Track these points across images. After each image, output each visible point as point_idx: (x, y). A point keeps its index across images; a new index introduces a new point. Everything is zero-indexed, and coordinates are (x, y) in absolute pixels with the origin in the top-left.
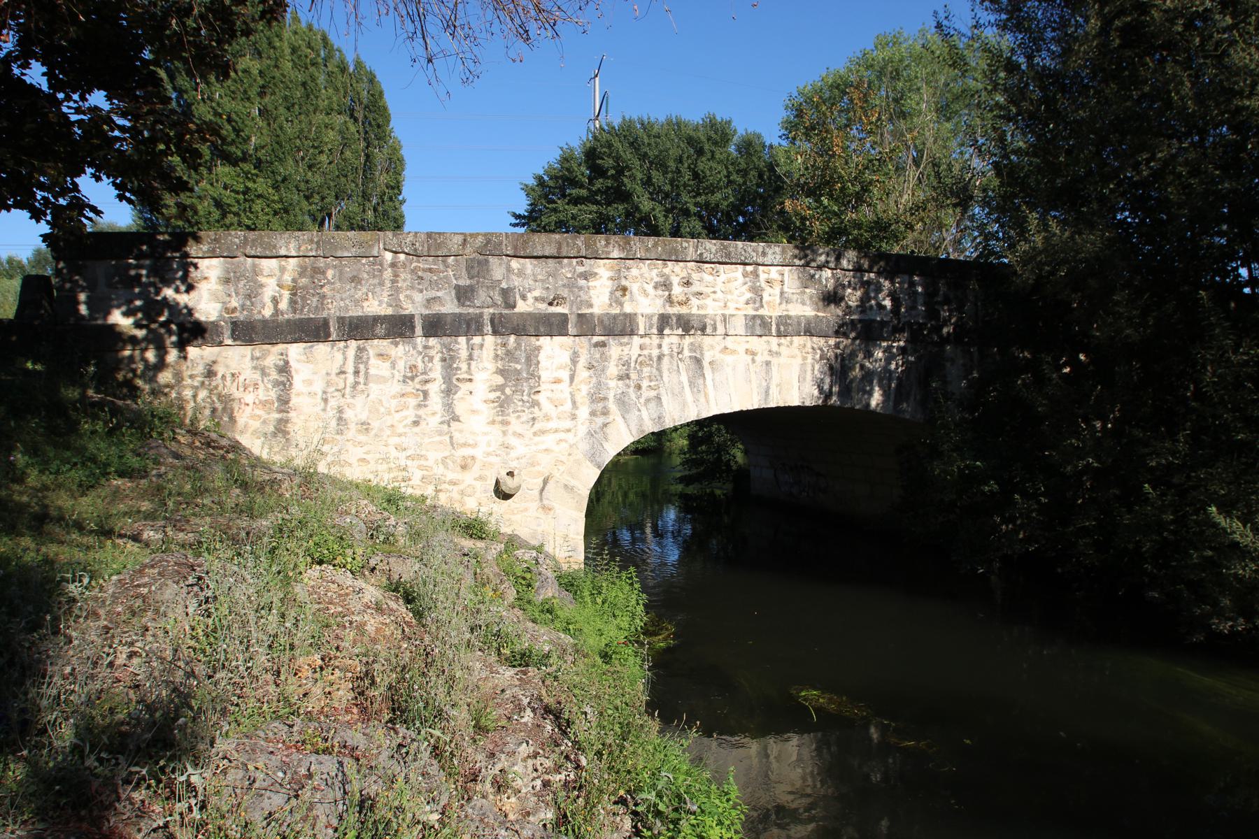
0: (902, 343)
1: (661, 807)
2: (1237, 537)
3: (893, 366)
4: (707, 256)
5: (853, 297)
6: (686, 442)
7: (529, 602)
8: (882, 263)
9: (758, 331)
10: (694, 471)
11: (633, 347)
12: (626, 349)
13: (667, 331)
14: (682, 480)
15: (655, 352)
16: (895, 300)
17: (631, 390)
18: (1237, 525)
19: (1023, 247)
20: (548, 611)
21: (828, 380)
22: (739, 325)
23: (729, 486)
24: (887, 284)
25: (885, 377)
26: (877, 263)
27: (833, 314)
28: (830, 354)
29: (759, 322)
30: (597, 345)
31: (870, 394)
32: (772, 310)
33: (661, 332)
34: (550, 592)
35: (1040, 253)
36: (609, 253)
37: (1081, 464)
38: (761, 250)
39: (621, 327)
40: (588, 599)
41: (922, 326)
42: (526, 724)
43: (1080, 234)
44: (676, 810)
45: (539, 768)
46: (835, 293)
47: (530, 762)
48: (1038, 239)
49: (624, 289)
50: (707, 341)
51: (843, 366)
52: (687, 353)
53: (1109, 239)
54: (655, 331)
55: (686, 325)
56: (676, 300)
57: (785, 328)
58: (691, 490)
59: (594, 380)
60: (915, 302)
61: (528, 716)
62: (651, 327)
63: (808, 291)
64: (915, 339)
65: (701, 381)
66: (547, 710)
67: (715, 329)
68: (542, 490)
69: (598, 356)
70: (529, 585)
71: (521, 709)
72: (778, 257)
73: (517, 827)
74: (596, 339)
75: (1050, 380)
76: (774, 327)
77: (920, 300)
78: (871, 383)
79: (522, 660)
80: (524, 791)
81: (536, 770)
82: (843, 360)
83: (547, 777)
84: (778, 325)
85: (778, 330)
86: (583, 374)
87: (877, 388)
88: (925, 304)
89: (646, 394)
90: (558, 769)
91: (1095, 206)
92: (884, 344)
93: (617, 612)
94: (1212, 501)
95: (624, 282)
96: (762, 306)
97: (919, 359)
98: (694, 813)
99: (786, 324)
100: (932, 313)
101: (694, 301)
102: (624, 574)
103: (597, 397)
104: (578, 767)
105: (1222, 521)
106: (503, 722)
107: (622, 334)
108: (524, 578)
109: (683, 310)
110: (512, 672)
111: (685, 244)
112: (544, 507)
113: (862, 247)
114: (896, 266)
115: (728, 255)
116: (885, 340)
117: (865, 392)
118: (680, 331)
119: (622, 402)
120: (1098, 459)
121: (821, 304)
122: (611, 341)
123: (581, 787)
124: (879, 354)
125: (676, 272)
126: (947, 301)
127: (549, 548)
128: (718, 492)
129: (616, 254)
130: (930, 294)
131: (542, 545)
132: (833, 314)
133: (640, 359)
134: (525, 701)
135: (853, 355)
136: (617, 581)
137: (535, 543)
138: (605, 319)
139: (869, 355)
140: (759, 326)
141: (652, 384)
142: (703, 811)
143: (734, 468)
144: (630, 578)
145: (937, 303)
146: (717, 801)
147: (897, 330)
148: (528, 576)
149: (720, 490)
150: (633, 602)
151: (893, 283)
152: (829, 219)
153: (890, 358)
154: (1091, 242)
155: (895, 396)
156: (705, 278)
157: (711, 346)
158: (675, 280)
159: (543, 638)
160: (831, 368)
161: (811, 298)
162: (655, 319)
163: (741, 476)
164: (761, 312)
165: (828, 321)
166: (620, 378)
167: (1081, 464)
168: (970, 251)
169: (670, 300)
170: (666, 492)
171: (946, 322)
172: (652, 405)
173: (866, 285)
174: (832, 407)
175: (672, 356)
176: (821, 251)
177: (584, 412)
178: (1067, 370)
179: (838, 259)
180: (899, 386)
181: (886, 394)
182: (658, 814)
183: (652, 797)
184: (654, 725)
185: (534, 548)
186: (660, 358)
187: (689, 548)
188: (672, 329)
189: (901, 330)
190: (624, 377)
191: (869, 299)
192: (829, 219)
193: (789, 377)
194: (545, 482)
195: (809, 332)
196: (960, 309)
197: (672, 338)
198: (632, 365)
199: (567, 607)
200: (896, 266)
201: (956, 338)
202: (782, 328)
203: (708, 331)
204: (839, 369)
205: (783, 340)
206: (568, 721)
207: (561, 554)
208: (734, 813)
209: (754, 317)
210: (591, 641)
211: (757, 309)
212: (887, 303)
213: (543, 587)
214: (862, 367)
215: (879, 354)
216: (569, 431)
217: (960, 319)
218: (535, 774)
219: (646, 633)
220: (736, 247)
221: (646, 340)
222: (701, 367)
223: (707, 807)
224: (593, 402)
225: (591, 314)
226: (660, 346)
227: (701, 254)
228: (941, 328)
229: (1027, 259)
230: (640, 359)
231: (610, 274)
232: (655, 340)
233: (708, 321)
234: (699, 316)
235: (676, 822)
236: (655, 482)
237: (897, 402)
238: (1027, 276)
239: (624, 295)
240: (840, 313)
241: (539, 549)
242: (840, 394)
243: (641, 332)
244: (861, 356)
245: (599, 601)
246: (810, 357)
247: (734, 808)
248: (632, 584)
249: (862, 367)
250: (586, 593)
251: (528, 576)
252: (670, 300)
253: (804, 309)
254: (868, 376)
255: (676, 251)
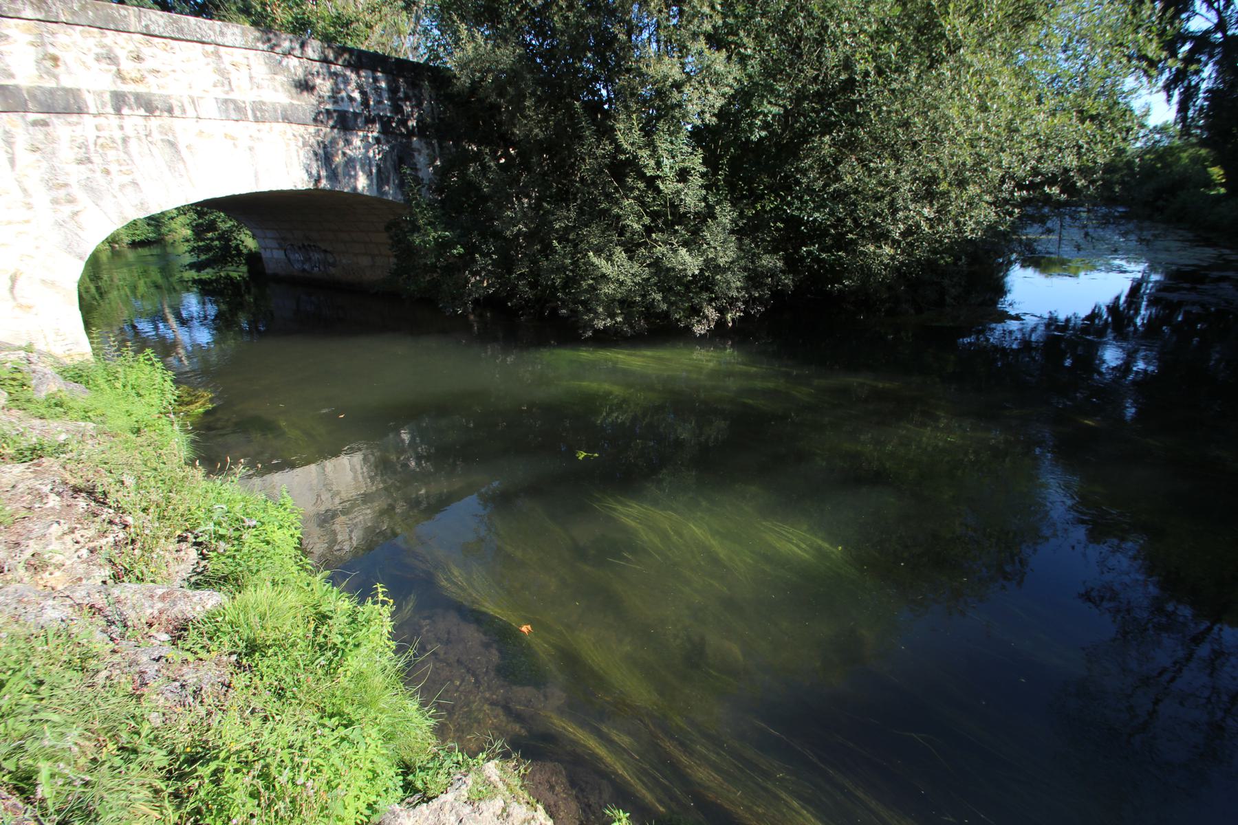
0: (375, 134)
1: (222, 531)
2: (604, 270)
3: (371, 154)
4: (154, 29)
5: (324, 86)
6: (189, 232)
7: (29, 401)
8: (346, 56)
9: (233, 115)
10: (203, 257)
11: (86, 127)
12: (79, 128)
13: (125, 111)
14: (192, 266)
15: (118, 135)
16: (363, 93)
17: (98, 175)
18: (604, 262)
19: (458, 54)
20: (56, 405)
21: (314, 165)
22: (209, 107)
23: (244, 269)
24: (354, 76)
25: (366, 163)
26: (341, 55)
27: (307, 102)
28: (312, 141)
29: (232, 106)
30: (35, 123)
31: (355, 177)
32: (245, 94)
33: (118, 111)
34: (55, 386)
35: (471, 61)
36: (19, 11)
37: (516, 229)
38: (218, 29)
39: (64, 104)
40: (105, 386)
41: (390, 120)
42: (52, 508)
43: (499, 48)
44: (237, 529)
45: (81, 540)
46: (306, 82)
47: (68, 538)
48: (470, 47)
49: (55, 59)
50: (177, 124)
51: (326, 153)
52: (156, 136)
53: (520, 55)
54: (110, 110)
55: (148, 106)
56: (128, 76)
57: (260, 114)
58: (207, 274)
59: (44, 164)
60: (380, 96)
61: (53, 501)
62: (104, 105)
63: (277, 77)
64: (386, 129)
65: (181, 165)
66: (77, 490)
67: (184, 111)
68: (12, 288)
69: (41, 137)
70: (23, 385)
71: (42, 497)
72: (239, 39)
73: (67, 593)
74: (32, 117)
75: (490, 167)
76: (250, 113)
77: (385, 95)
78: (354, 168)
79: (33, 454)
80: (68, 563)
81: (77, 542)
82: (325, 147)
83: (92, 545)
84: (253, 110)
85: (255, 116)
86: (24, 157)
87: (361, 173)
88: (389, 99)
89: (118, 179)
90: (103, 534)
91: (507, 25)
92: (361, 133)
93: (142, 392)
94: (591, 249)
95: (51, 50)
96: (232, 90)
97: (392, 148)
98: (255, 527)
99: (262, 110)
100: (397, 109)
101: (150, 78)
102: (141, 357)
103: (55, 184)
104: (126, 526)
105: (595, 260)
106: (23, 513)
107: (67, 111)
108: (14, 379)
109: (141, 89)
110: (22, 467)
111: (123, 12)
112: (21, 306)
113: (327, 39)
114: (363, 61)
115: (181, 30)
116: (360, 129)
117: (351, 176)
118: (142, 112)
119: (89, 187)
120: (526, 225)
121: (294, 90)
122: (53, 118)
123: (133, 541)
124: (357, 142)
125: (122, 44)
126: (407, 98)
127: (40, 346)
128: (234, 274)
129: (29, 12)
130: (393, 91)
131: (31, 345)
132: (307, 102)
133: (100, 141)
134: (46, 489)
135: (333, 142)
136: (135, 364)
137: (24, 344)
138: (38, 93)
139: (348, 142)
140: (234, 110)
141: (124, 168)
142: (263, 523)
143: (245, 251)
144: (150, 359)
145: (400, 99)
146: (275, 513)
147: (369, 121)
148: (19, 376)
149: (238, 272)
150: (159, 380)
151: (359, 76)
152: (291, 8)
153: (368, 147)
154: (507, 55)
155: (380, 178)
156: (156, 53)
157: (182, 128)
158: (122, 54)
159: (58, 430)
160: (316, 154)
161: (282, 85)
162: (107, 97)
163: (253, 259)
164: (232, 96)
165: (304, 110)
166: (80, 162)
167: (516, 229)
168: (420, 57)
169: (119, 75)
170: (181, 281)
171: (410, 116)
172: (130, 190)
173: (334, 75)
174: (323, 190)
175: (139, 139)
176: (283, 36)
177: (41, 197)
178: (503, 161)
179: (303, 45)
180: (379, 170)
181: (369, 175)
182: (222, 537)
183: (211, 527)
184: (199, 473)
185: (20, 348)
186: (125, 140)
187: (222, 324)
188: (131, 108)
189: (373, 121)
190: (85, 161)
191: (339, 91)
192: (291, 8)
193: (280, 162)
194: (14, 279)
195: (287, 119)
196: (419, 105)
197: (134, 119)
198: (92, 147)
199: (79, 396)
200: (363, 61)
201: (421, 130)
202: (259, 114)
203: (177, 112)
204: (325, 155)
205: (261, 125)
206: (104, 493)
207: (58, 351)
208: (292, 517)
209: (226, 101)
210: (119, 422)
211: (227, 93)
212: (356, 95)
213: (42, 383)
214: (344, 154)
215: (357, 142)
216: (27, 222)
217: (420, 115)
218: (77, 546)
219: (180, 402)
220: (188, 22)
221: (101, 120)
222: (178, 151)
223: (265, 520)
224: (50, 188)
225: (16, 87)
226: (122, 128)
227: (147, 26)
228: (406, 121)
229: (463, 66)
230: (100, 141)
231: (31, 38)
232: (114, 120)
233: (175, 103)
234: (161, 96)
235: (238, 539)
236: (165, 270)
237: (380, 187)
238: (464, 80)
239: (57, 66)
240: (315, 103)
241: (29, 349)
242: (328, 178)
243: (93, 110)
244: (341, 143)
245: (119, 385)
246: (293, 143)
247: (291, 513)
248: (152, 365)
249: (344, 154)
250: (101, 381)
251: (19, 376)
252: (119, 75)
253: (279, 94)
254: (350, 162)
255: (114, 20)
